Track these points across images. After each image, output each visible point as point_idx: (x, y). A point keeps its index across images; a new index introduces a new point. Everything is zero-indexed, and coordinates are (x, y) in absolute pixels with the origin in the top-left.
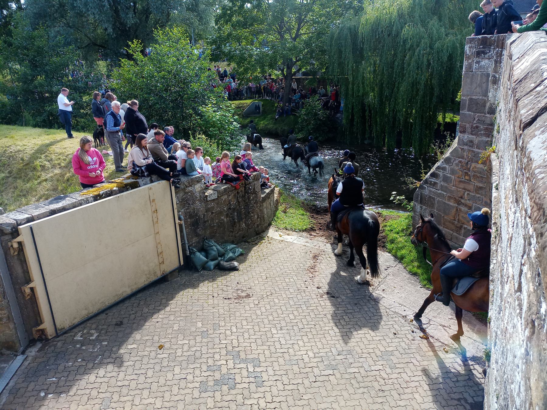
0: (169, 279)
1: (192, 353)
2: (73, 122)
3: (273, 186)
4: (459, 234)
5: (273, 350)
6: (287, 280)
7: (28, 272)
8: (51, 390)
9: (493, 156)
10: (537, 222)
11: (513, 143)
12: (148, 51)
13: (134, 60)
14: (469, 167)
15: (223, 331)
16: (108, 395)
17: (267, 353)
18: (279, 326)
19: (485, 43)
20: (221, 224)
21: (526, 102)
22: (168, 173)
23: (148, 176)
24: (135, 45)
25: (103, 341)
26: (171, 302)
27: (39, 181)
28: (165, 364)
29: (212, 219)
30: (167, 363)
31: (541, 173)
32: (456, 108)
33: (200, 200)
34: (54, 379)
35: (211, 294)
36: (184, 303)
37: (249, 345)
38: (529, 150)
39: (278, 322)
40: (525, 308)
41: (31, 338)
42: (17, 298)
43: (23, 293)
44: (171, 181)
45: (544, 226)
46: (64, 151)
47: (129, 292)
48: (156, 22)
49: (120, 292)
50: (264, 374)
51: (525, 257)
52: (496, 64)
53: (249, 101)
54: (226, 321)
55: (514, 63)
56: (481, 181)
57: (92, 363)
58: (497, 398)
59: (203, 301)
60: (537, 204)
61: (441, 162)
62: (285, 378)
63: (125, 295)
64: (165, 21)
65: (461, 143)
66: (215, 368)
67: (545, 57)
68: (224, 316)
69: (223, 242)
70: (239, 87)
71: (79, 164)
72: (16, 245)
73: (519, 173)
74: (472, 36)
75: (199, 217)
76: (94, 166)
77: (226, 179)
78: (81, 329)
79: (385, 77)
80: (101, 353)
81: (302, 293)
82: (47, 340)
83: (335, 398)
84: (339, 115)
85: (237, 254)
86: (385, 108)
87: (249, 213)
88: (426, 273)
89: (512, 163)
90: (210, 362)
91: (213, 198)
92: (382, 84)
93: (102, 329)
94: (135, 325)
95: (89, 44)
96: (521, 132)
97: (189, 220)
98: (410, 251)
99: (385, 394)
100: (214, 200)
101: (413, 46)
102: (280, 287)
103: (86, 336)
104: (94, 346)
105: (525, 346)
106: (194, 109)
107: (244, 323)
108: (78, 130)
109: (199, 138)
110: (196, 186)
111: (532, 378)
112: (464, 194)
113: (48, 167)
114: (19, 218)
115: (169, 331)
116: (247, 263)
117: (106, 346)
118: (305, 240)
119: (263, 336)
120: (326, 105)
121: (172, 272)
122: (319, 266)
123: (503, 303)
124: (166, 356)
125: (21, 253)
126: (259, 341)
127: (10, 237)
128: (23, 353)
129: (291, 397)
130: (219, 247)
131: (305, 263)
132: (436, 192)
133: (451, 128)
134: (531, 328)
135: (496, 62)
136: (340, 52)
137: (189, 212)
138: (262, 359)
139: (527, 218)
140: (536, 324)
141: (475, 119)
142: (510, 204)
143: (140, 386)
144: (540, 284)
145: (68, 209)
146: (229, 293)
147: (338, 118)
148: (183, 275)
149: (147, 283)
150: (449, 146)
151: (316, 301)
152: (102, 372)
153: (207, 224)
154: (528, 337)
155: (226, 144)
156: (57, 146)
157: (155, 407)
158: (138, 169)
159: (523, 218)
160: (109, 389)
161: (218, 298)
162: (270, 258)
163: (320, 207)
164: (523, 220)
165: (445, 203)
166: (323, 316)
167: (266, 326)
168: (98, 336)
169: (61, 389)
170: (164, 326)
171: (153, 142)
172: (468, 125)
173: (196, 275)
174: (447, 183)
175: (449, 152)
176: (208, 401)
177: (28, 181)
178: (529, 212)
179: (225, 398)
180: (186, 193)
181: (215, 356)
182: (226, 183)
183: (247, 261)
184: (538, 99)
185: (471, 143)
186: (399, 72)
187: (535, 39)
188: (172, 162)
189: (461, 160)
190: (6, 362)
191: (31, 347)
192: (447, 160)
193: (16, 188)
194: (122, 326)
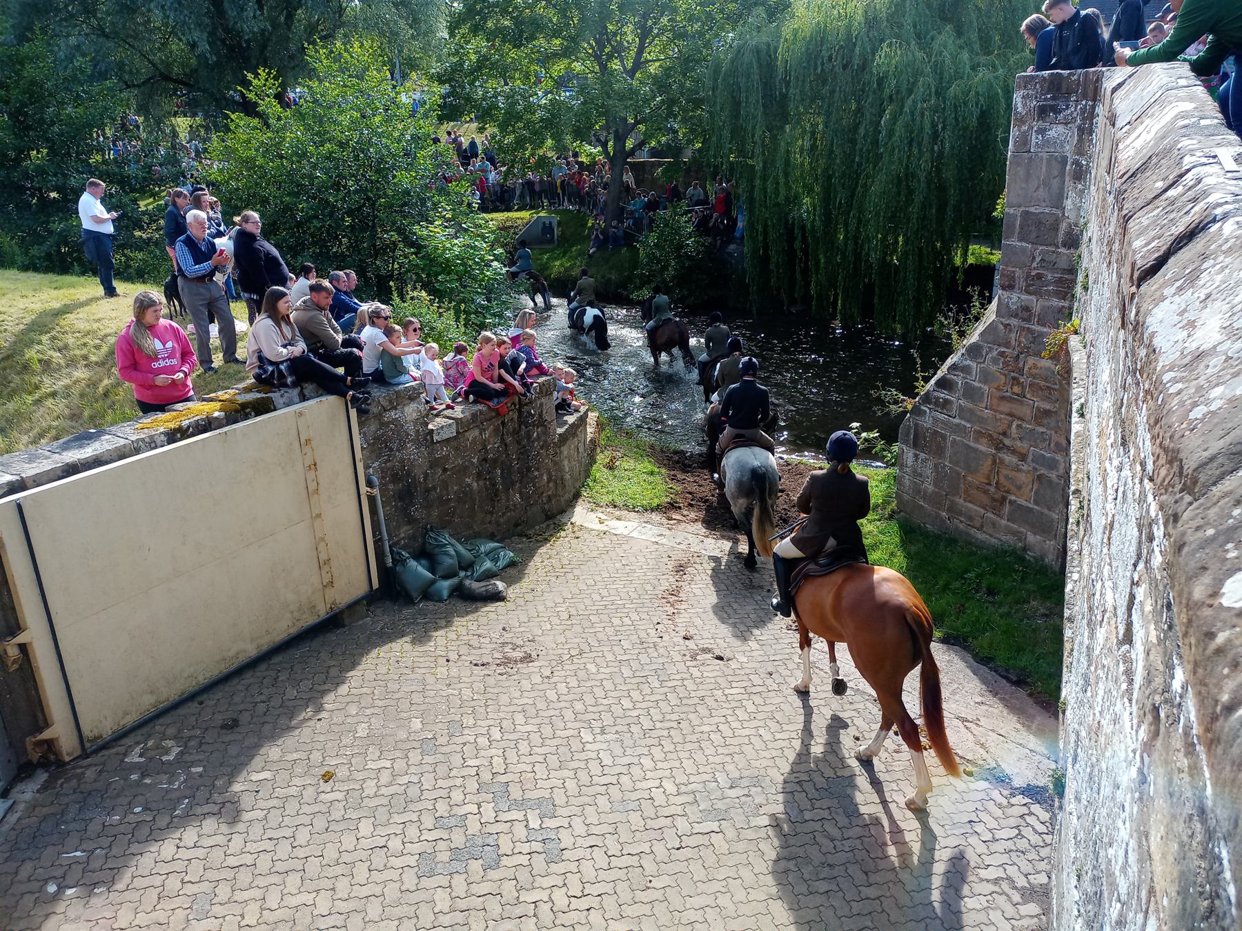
0: (347, 621)
1: (401, 790)
2: (117, 259)
3: (583, 409)
6: (616, 621)
7: (14, 609)
9: (1074, 341)
10: (1166, 490)
11: (1116, 314)
12: (292, 95)
14: (1021, 365)
15: (472, 739)
16: (205, 887)
17: (571, 785)
18: (599, 724)
22: (342, 379)
24: (261, 82)
25: (193, 764)
27: (37, 396)
28: (337, 815)
30: (343, 812)
31: (1175, 381)
32: (991, 232)
33: (417, 442)
34: (78, 854)
35: (443, 654)
36: (379, 677)
37: (529, 768)
38: (1151, 330)
40: (1138, 679)
41: (23, 760)
44: (349, 398)
45: (1182, 498)
46: (95, 326)
47: (252, 651)
48: (311, 29)
50: (564, 834)
51: (1141, 566)
53: (525, 214)
55: (1120, 134)
57: (165, 816)
58: (1079, 876)
59: (423, 671)
60: (1166, 450)
61: (959, 354)
62: (610, 841)
63: (243, 659)
64: (334, 22)
65: (1003, 311)
66: (453, 822)
68: (473, 703)
69: (470, 537)
71: (132, 358)
73: (1129, 380)
74: (1030, 71)
77: (477, 392)
78: (139, 738)
80: (188, 792)
82: (61, 764)
83: (724, 883)
84: (732, 247)
85: (501, 564)
89: (1114, 359)
90: (442, 808)
91: (445, 437)
92: (830, 177)
93: (190, 738)
94: (267, 727)
96: (1134, 289)
97: (391, 487)
98: (892, 554)
100: (448, 440)
102: (601, 636)
103: (153, 753)
104: (173, 777)
105: (1138, 764)
106: (400, 231)
107: (520, 719)
108: (128, 279)
109: (412, 298)
110: (406, 409)
111: (1153, 833)
112: (1010, 426)
113: (59, 364)
116: (525, 584)
117: (201, 776)
118: (656, 530)
119: (562, 749)
120: (703, 226)
121: (352, 606)
122: (687, 588)
123: (1093, 669)
124: (340, 796)
130: (460, 548)
131: (656, 582)
132: (949, 422)
133: (983, 276)
134: (1151, 724)
135: (1081, 130)
136: (736, 104)
138: (560, 799)
139: (1146, 481)
140: (1162, 715)
142: (1110, 450)
143: (280, 866)
144: (1170, 627)
145: (107, 463)
146: (483, 651)
148: (378, 612)
149: (294, 631)
150: (977, 319)
151: (681, 667)
153: (433, 495)
154: (1145, 744)
155: (476, 313)
156: (80, 316)
157: (315, 913)
158: (270, 368)
159: (1137, 481)
161: (460, 663)
162: (576, 572)
164: (1138, 486)
167: (569, 725)
168: (182, 753)
169: (97, 877)
170: (336, 729)
171: (306, 306)
172: (1018, 272)
173: (407, 612)
175: (978, 332)
176: (436, 897)
178: (1150, 467)
179: (475, 889)
181: (453, 794)
182: (475, 402)
183: (526, 579)
184: (1172, 216)
185: (1025, 312)
186: (869, 151)
187: (1165, 80)
188: (351, 353)
191: (22, 780)
192: (974, 351)
194: (239, 729)
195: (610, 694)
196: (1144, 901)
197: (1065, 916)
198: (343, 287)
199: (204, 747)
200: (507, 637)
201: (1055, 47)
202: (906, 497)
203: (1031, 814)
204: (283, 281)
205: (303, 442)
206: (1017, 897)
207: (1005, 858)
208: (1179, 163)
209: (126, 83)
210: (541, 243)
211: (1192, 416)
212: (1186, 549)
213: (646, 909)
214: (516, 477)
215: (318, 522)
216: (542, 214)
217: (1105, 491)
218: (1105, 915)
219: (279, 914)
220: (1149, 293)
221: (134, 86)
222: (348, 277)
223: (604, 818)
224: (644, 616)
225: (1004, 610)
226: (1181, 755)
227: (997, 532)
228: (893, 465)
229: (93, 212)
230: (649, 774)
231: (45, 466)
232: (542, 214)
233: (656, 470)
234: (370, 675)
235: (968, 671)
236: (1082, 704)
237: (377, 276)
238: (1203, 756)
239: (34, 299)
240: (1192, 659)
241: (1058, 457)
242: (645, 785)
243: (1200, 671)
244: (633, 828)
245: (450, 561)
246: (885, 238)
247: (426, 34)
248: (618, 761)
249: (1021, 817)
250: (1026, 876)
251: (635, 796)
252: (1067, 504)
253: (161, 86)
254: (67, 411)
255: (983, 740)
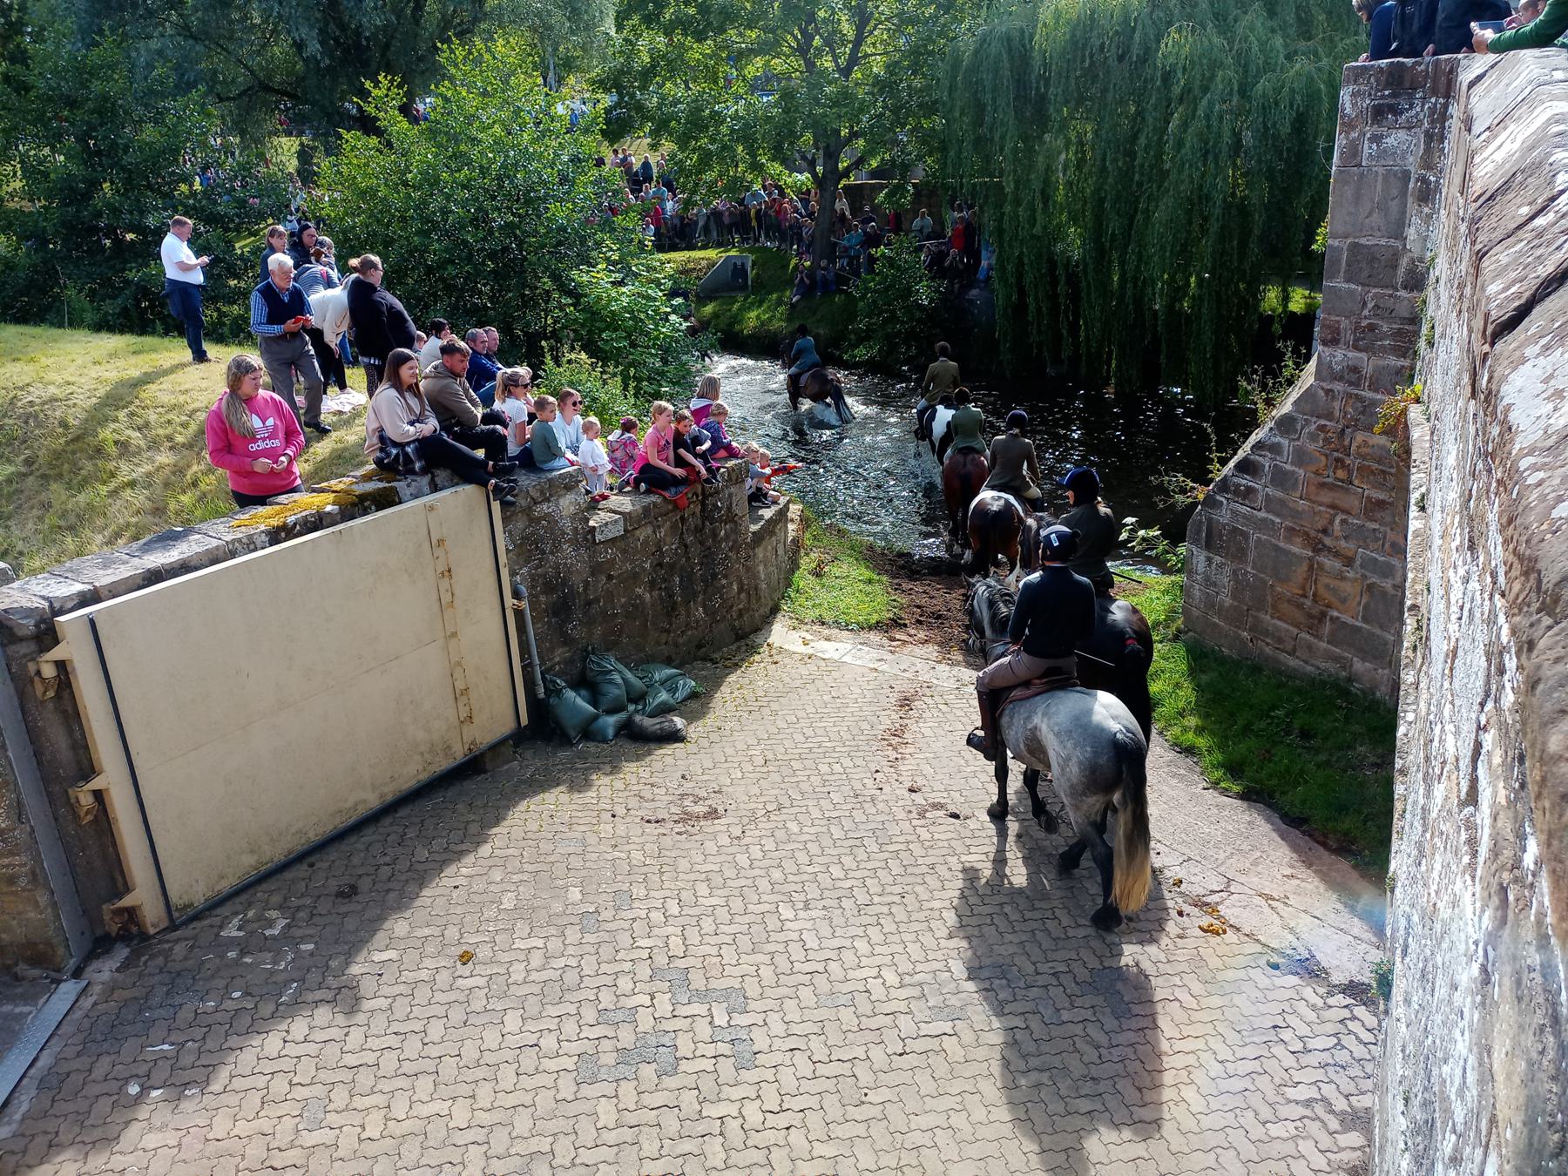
0: (489, 766)
1: (555, 975)
2: (208, 315)
3: (783, 500)
4: (1316, 637)
5: (783, 965)
6: (824, 769)
7: (87, 748)
8: (159, 1075)
9: (1415, 413)
10: (1520, 610)
11: (1466, 379)
12: (421, 107)
13: (379, 132)
14: (1346, 443)
15: (643, 914)
16: (318, 1090)
17: (767, 972)
18: (802, 897)
19: (1398, 82)
20: (635, 610)
21: (1504, 259)
22: (482, 464)
23: (424, 471)
24: (383, 93)
25: (303, 940)
26: (495, 830)
27: (113, 485)
28: (477, 1005)
29: (610, 596)
30: (484, 1002)
31: (1535, 468)
32: (1311, 270)
33: (574, 542)
34: (166, 1047)
35: (608, 807)
36: (530, 835)
37: (714, 951)
38: (1506, 401)
39: (798, 887)
40: (1483, 851)
41: (99, 932)
42: (56, 820)
43: (73, 807)
44: (490, 488)
45: (1539, 621)
46: (182, 399)
47: (373, 801)
48: (446, 23)
49: (349, 804)
50: (757, 1034)
51: (1490, 706)
52: (1428, 144)
53: (711, 254)
54: (651, 885)
55: (1476, 143)
56: (1380, 481)
57: (270, 1003)
58: (1406, 1100)
59: (583, 828)
60: (1521, 558)
61: (1267, 429)
62: (815, 1043)
63: (362, 811)
64: (468, 21)
65: (1324, 373)
66: (620, 1016)
67: (1562, 127)
68: (645, 870)
69: (642, 661)
70: (686, 209)
71: (225, 439)
72: (49, 671)
73: (1480, 465)
74: (1362, 60)
75: (571, 588)
76: (269, 444)
77: (650, 478)
78: (239, 907)
79: (1110, 180)
80: (296, 975)
81: (866, 805)
82: (144, 937)
83: (959, 1099)
84: (974, 292)
85: (680, 695)
86: (1110, 277)
87: (714, 576)
88: (1222, 747)
89: (1462, 438)
90: (607, 999)
91: (611, 536)
92: (1102, 201)
93: (298, 908)
94: (392, 895)
95: (250, 89)
96: (1486, 348)
97: (543, 598)
98: (1177, 686)
99: (1101, 1088)
100: (613, 540)
101: (1190, 90)
102: (805, 786)
103: (255, 925)
104: (278, 957)
105: (1481, 960)
106: (556, 277)
107: (703, 889)
108: (220, 340)
109: (569, 362)
110: (562, 501)
111: (1496, 1047)
112: (1331, 522)
113: (138, 447)
114: (58, 594)
115: (490, 913)
116: (710, 720)
117: (312, 954)
118: (875, 654)
119: (755, 928)
120: (937, 265)
121: (495, 747)
122: (914, 727)
123: (1428, 835)
124: (482, 982)
125: (66, 694)
126: (744, 943)
127: (32, 646)
128: (77, 974)
129: (836, 1097)
130: (629, 675)
131: (874, 719)
132: (1253, 516)
133: (1300, 329)
134: (1497, 909)
135: (1429, 137)
136: (980, 108)
137: (544, 576)
138: (752, 990)
139: (1497, 597)
140: (1511, 898)
141: (1365, 304)
142: (1455, 555)
143: (408, 1067)
144: (1523, 786)
145: (197, 569)
146: (658, 804)
147: (971, 302)
148: (528, 754)
149: (424, 777)
150: (1290, 383)
151: (906, 826)
152: (299, 1027)
153: (595, 609)
154: (1490, 934)
155: (649, 379)
156: (164, 386)
157: (451, 1125)
158: (394, 451)
159: (1486, 596)
160: (322, 1075)
161: (629, 819)
162: (774, 706)
163: (920, 560)
164: (1487, 603)
165: (1277, 548)
166: (925, 869)
167: (764, 898)
168: (288, 926)
169: (185, 1078)
170: (476, 898)
171: (437, 373)
172: (1345, 323)
173: (563, 754)
174: (1285, 490)
175: (1292, 399)
176: (600, 1110)
177: (81, 487)
178: (1501, 579)
179: (647, 1099)
180: (534, 521)
181: (620, 982)
182: (648, 492)
183: (711, 715)
184: (1539, 252)
185: (1353, 374)
186: (1151, 167)
187: (1537, 72)
188: (494, 431)
189: (1323, 422)
190: (30, 999)
191: (98, 957)
192: (1286, 424)
193: (46, 506)
194: (356, 898)
195: (816, 859)
196: (1484, 1133)
197: (1389, 1149)
198: (479, 348)
199: (315, 919)
200: (688, 786)
201: (1395, 28)
202: (1196, 613)
203: (1354, 1018)
204: (409, 341)
205: (434, 541)
206: (1334, 1124)
207: (1319, 1074)
208: (1551, 182)
209: (218, 95)
210: (732, 289)
211: (1555, 514)
212: (1541, 687)
213: (861, 1130)
214: (699, 587)
215: (453, 642)
216: (733, 253)
217: (1448, 607)
218: (1437, 1149)
219: (407, 1126)
220: (1506, 354)
221: (229, 99)
222: (490, 336)
223: (807, 1014)
224: (860, 762)
225: (1322, 757)
226: (1532, 949)
227: (1315, 656)
228: (1179, 571)
229: (179, 258)
230: (864, 961)
231: (123, 572)
232: (733, 253)
233: (876, 577)
234: (517, 833)
235: (1274, 835)
236: (1414, 880)
237: (526, 334)
238: (1558, 952)
239: (108, 366)
240: (1545, 827)
241: (1395, 561)
242: (860, 974)
243: (1555, 843)
244: (844, 1028)
245: (617, 691)
246: (1172, 277)
247: (587, 28)
248: (826, 943)
249: (1341, 1021)
250: (1347, 1097)
251: (846, 988)
252: (1403, 623)
253: (257, 101)
254: (148, 505)
255: (1292, 924)
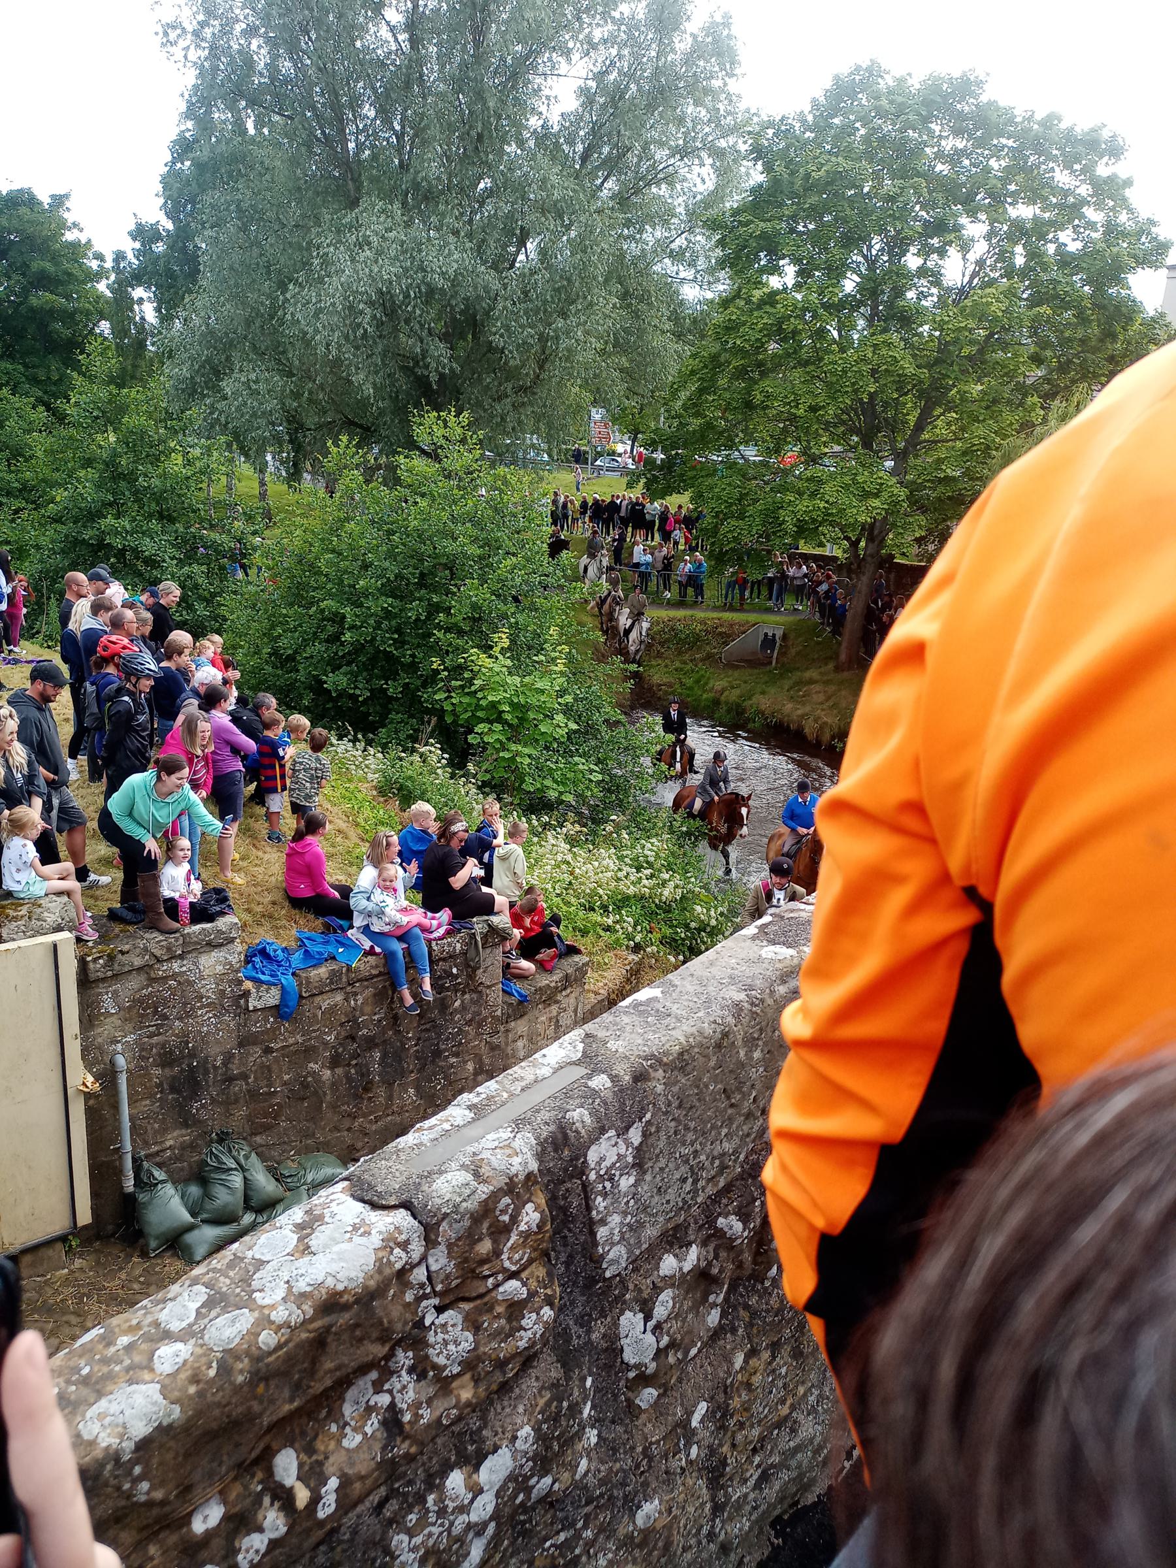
33: (217, 1007)
87: (437, 1054)
153: (239, 1087)
173: (137, 1265)
